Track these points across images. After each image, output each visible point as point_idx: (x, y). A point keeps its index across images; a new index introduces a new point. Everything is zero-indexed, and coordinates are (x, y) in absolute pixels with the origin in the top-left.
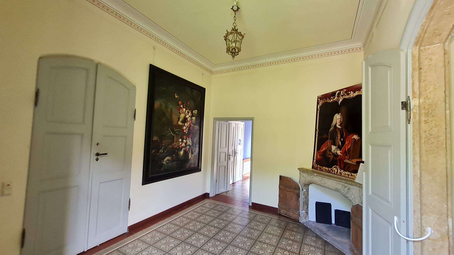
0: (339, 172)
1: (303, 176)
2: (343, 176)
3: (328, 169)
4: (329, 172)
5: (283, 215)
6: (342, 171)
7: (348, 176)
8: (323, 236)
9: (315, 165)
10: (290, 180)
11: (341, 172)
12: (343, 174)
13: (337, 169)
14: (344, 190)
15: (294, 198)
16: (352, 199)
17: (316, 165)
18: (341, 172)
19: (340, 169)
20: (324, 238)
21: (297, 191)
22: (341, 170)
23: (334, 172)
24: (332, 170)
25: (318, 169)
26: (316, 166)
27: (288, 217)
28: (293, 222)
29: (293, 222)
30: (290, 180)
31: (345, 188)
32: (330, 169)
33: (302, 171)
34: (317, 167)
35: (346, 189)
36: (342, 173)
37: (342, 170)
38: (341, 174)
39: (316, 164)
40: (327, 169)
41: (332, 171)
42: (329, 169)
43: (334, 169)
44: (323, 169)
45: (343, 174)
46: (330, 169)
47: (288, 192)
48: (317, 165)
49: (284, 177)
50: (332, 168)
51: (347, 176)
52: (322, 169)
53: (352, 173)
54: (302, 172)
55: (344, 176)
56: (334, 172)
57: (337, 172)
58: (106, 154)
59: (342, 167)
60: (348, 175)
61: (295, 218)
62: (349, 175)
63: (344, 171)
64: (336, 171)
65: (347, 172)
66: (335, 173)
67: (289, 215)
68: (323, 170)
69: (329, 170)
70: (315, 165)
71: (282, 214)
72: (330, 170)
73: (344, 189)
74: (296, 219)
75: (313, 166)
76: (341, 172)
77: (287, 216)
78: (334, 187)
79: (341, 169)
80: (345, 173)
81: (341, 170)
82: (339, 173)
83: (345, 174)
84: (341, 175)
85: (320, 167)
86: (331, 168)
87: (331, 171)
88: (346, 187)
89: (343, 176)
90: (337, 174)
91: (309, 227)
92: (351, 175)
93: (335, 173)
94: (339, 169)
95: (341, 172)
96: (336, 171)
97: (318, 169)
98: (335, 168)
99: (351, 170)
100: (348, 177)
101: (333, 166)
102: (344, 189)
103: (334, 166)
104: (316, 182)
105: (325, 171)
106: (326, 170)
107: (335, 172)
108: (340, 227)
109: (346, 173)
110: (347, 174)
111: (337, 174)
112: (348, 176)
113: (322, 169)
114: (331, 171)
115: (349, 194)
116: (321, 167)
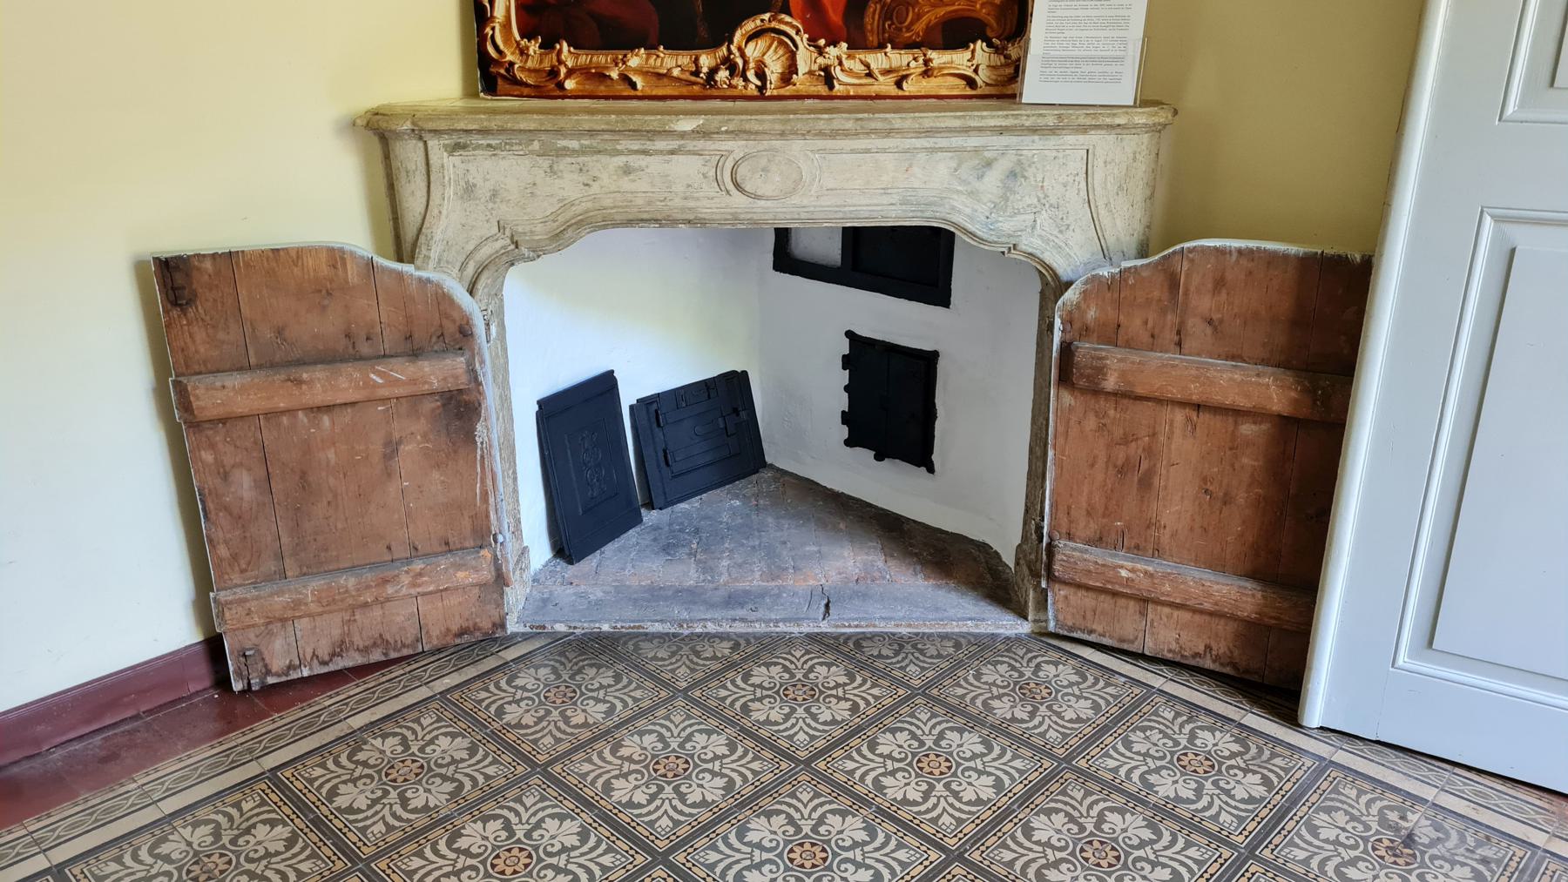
0: (803, 68)
1: (469, 190)
2: (848, 97)
3: (685, 59)
4: (704, 88)
5: (306, 673)
6: (832, 51)
7: (899, 84)
8: (767, 622)
9: (523, 52)
10: (325, 270)
11: (826, 69)
12: (850, 72)
13: (781, 43)
14: (971, 194)
15: (406, 448)
16: (1047, 241)
17: (534, 47)
18: (826, 69)
19: (812, 41)
20: (782, 628)
21: (437, 372)
22: (821, 52)
23: (751, 75)
24: (732, 68)
25: (561, 86)
26: (530, 64)
27: (376, 656)
28: (471, 672)
29: (471, 672)
30: (325, 270)
31: (980, 177)
32: (706, 61)
33: (447, 140)
34: (546, 65)
35: (993, 179)
36: (837, 72)
37: (833, 42)
38: (829, 80)
39: (527, 34)
40: (673, 62)
41: (732, 68)
42: (696, 61)
43: (752, 50)
44: (625, 78)
45: (850, 72)
46: (706, 61)
47: (326, 420)
48: (547, 45)
49: (229, 258)
50: (731, 42)
51: (885, 85)
52: (614, 74)
53: (932, 54)
54: (457, 147)
55: (862, 91)
56: (751, 75)
57: (792, 68)
58: (1552, 84)
59: (835, 17)
60: (891, 79)
61: (455, 628)
62: (905, 77)
63: (858, 43)
64: (774, 69)
65: (880, 55)
66: (762, 88)
67: (381, 641)
68: (633, 85)
69: (696, 73)
70: (523, 52)
71: (294, 675)
72: (713, 71)
73: (977, 185)
74: (460, 634)
75: (498, 63)
76: (821, 60)
77: (365, 650)
78: (885, 191)
79: (822, 32)
80: (868, 66)
81: (821, 52)
82: (811, 73)
83: (870, 75)
84: (831, 87)
85: (584, 59)
86: (717, 45)
87: (723, 74)
88: (989, 164)
89: (848, 97)
90: (788, 90)
91: (606, 628)
92: (927, 73)
93: (762, 88)
94: (802, 41)
95: (821, 60)
96: (774, 69)
97: (570, 84)
98: (762, 43)
99: (920, 27)
100: (894, 91)
101: (737, 24)
102: (977, 185)
103: (750, 26)
104: (678, 202)
105: (660, 92)
106: (667, 76)
107: (761, 75)
108: (683, 506)
109: (877, 60)
110: (886, 66)
111: (788, 90)
112: (899, 84)
113: (614, 74)
114: (723, 74)
115: (1017, 213)
116: (602, 58)
